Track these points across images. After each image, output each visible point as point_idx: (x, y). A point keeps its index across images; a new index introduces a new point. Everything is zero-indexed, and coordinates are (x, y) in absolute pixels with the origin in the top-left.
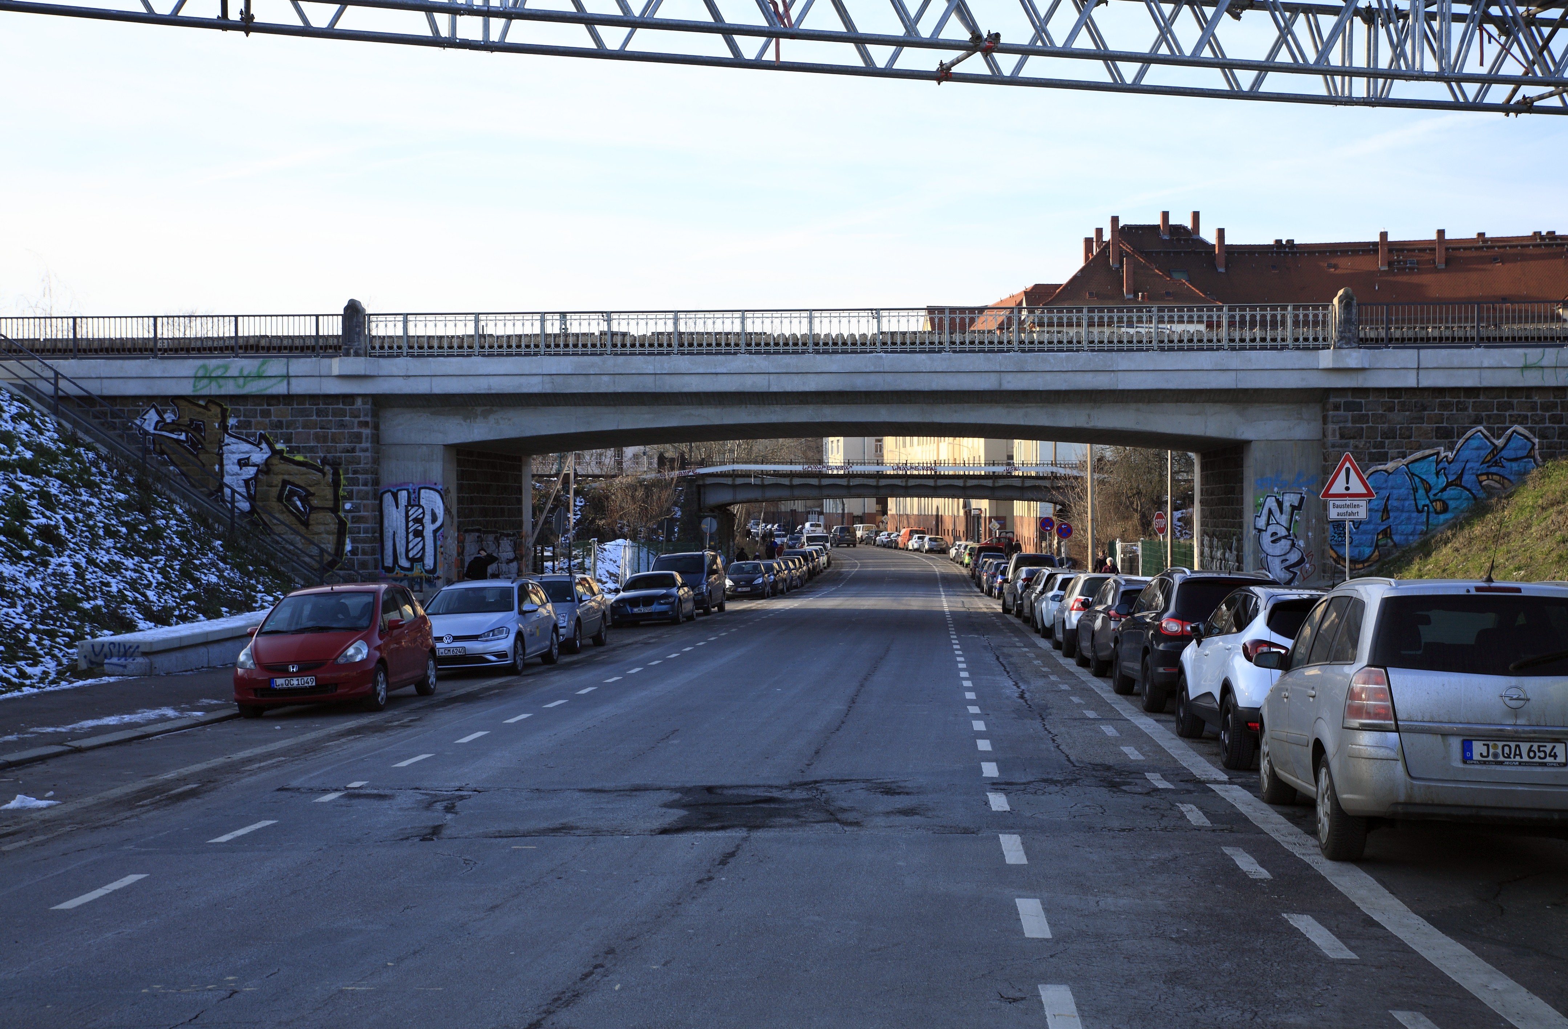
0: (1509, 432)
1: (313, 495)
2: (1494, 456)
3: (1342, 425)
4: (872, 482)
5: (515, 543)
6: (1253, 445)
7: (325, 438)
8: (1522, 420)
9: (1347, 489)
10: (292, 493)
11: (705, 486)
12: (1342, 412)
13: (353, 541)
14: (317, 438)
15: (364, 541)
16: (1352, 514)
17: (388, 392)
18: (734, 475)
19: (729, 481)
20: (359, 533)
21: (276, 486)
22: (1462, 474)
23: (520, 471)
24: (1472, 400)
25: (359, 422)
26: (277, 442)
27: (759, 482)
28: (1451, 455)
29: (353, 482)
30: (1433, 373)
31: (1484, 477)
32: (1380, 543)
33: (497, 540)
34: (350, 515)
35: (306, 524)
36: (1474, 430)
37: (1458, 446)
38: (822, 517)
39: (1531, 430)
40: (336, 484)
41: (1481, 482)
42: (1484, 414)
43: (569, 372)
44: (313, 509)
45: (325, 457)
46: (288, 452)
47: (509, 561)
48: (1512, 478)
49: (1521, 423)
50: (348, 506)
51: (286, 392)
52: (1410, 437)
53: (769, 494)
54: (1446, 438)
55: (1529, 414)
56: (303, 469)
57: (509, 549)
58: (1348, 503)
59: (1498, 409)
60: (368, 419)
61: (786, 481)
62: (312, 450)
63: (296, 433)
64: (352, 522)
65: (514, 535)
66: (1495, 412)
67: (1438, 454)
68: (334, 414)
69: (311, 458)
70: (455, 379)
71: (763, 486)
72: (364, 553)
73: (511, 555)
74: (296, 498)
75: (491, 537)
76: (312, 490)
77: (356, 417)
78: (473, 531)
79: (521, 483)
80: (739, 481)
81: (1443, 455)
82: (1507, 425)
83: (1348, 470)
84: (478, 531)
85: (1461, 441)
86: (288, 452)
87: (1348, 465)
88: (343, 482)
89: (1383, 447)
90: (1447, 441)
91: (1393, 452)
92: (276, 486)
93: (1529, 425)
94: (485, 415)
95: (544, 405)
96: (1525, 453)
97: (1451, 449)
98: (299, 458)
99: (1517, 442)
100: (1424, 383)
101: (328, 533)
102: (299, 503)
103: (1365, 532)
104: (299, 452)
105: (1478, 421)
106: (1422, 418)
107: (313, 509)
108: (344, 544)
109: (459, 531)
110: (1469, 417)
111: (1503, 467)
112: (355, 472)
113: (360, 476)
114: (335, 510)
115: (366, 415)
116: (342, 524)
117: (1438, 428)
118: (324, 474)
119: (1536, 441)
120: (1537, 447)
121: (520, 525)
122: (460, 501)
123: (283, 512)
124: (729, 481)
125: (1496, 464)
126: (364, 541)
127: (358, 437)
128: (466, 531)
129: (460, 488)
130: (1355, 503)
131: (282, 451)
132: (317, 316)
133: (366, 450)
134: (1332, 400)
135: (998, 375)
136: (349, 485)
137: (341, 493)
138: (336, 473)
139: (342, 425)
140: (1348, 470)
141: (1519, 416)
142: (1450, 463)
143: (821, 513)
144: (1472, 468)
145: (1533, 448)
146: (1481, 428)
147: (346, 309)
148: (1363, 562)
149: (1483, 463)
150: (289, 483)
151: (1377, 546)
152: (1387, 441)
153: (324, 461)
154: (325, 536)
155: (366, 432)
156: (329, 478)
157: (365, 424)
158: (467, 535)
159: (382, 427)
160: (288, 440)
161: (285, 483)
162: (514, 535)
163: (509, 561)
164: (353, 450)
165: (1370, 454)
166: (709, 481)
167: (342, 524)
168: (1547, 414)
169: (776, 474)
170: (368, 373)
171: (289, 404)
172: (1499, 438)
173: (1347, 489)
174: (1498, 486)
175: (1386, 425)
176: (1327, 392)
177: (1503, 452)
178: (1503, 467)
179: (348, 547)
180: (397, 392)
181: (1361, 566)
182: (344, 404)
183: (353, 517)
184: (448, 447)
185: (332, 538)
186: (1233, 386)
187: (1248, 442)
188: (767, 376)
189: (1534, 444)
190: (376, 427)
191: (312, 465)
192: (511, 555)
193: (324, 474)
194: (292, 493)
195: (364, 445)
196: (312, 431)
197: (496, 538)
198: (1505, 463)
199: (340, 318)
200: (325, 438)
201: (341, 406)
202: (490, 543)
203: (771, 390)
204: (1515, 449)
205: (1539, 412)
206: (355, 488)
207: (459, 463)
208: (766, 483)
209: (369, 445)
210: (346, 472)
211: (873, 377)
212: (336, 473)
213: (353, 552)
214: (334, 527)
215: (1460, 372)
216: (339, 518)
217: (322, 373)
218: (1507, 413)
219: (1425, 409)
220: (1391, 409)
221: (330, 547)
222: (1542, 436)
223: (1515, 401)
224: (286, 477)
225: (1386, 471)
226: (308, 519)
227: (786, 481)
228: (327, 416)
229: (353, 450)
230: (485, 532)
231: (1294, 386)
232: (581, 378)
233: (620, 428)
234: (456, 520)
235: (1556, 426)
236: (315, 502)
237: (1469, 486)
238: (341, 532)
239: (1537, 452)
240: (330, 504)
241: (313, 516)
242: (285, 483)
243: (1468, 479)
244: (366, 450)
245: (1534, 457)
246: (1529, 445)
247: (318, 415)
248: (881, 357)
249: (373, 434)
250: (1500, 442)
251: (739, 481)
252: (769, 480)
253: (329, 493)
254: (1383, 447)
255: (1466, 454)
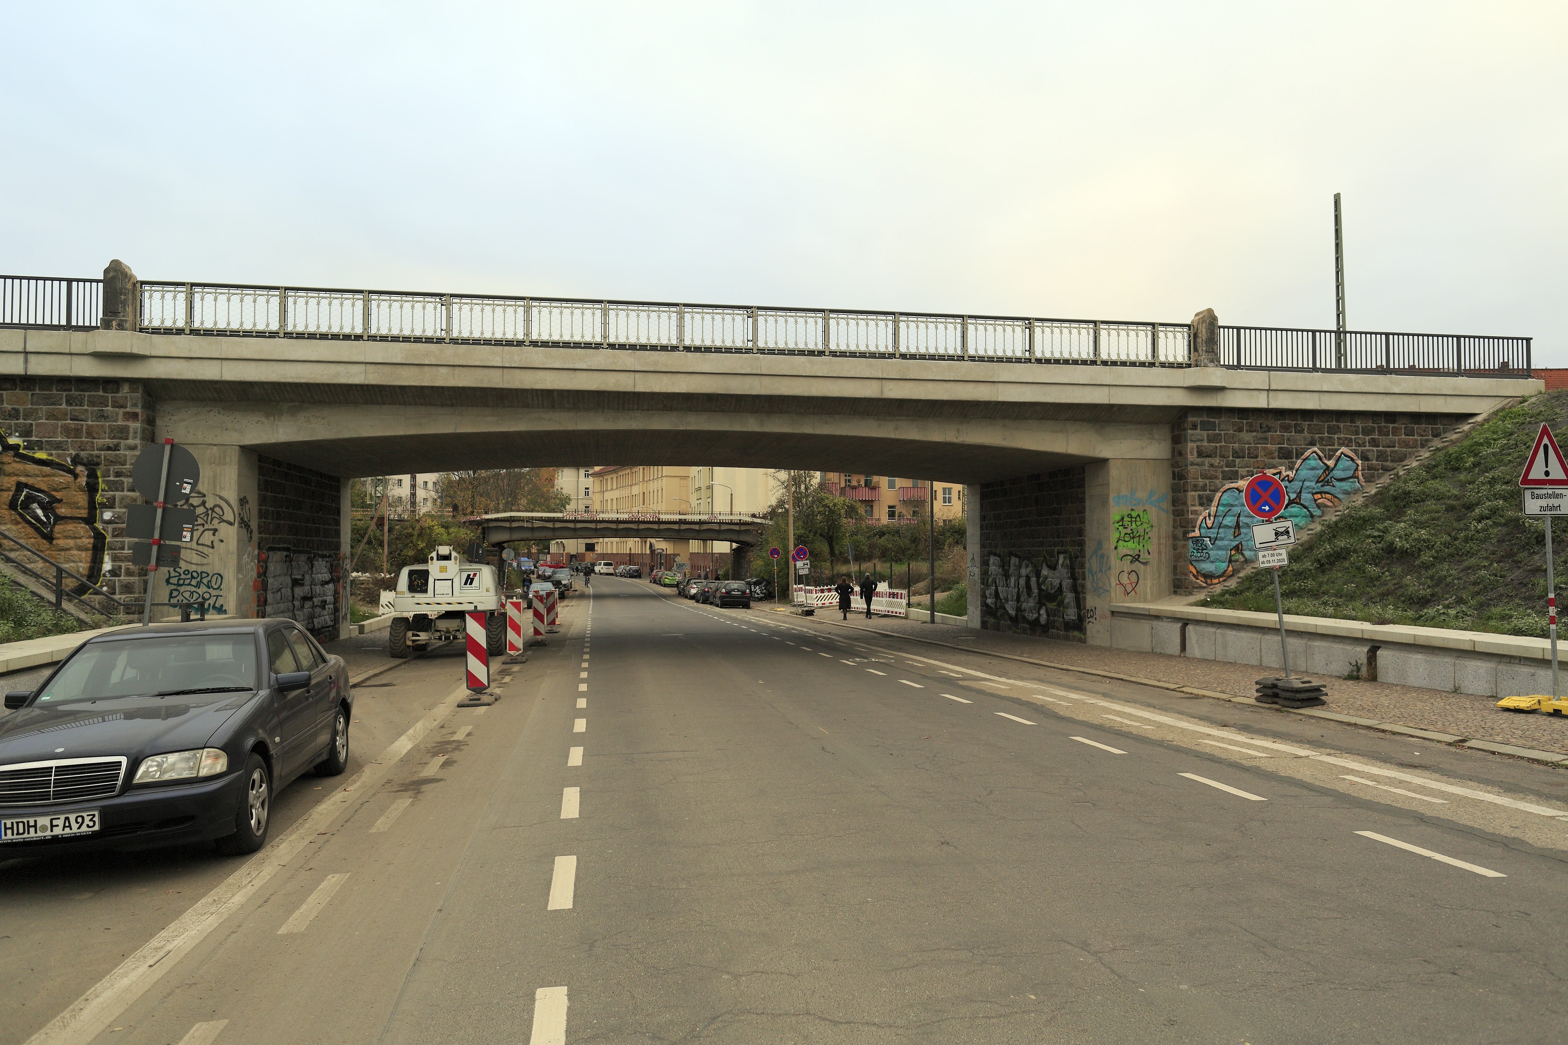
0: (1338, 453)
1: (60, 501)
2: (1327, 476)
3: (1199, 443)
4: (614, 526)
5: (332, 565)
6: (1111, 464)
7: (77, 432)
8: (1347, 443)
9: (1547, 473)
10: (30, 499)
11: (489, 528)
12: (1198, 431)
13: (114, 559)
14: (67, 431)
15: (127, 559)
16: (1553, 508)
17: (163, 376)
18: (511, 520)
19: (507, 525)
20: (123, 548)
21: (8, 490)
22: (1300, 492)
23: (339, 492)
24: (1307, 423)
25: (125, 414)
26: (10, 435)
27: (529, 525)
28: (1291, 474)
29: (115, 486)
30: (1281, 395)
31: (1319, 496)
32: (1233, 558)
33: (311, 561)
34: (110, 527)
35: (49, 538)
36: (1310, 451)
37: (1296, 466)
38: (549, 556)
39: (1355, 452)
40: (92, 489)
41: (1315, 500)
42: (1317, 436)
43: (399, 361)
44: (59, 519)
45: (77, 455)
46: (25, 448)
47: (325, 583)
48: (1341, 496)
49: (1347, 446)
50: (107, 515)
51: (22, 372)
52: (1256, 457)
53: (537, 535)
54: (1286, 458)
55: (1353, 437)
56: (47, 469)
57: (325, 570)
58: (1550, 492)
59: (1328, 433)
60: (138, 410)
61: (550, 525)
62: (58, 446)
63: (38, 425)
64: (114, 536)
65: (330, 556)
66: (1326, 434)
67: (1280, 473)
68: (92, 404)
69: (59, 456)
70: (253, 364)
71: (533, 529)
72: (129, 573)
73: (327, 576)
74: (35, 505)
75: (303, 558)
76: (58, 495)
77: (121, 407)
78: (279, 549)
79: (339, 504)
80: (515, 525)
81: (1284, 474)
82: (1336, 447)
83: (1546, 446)
84: (287, 549)
85: (1299, 461)
86: (25, 448)
87: (1546, 441)
88: (101, 486)
89: (1234, 466)
90: (1286, 461)
91: (1243, 471)
92: (8, 490)
93: (1354, 447)
94: (294, 411)
95: (366, 403)
96: (1350, 473)
97: (1291, 469)
98: (41, 455)
99: (1345, 463)
100: (1274, 405)
101: (80, 548)
102: (39, 512)
103: (1220, 548)
104: (41, 449)
105: (1313, 444)
106: (1266, 439)
107: (59, 519)
108: (101, 562)
109: (259, 548)
110: (1305, 438)
111: (1334, 486)
112: (118, 474)
113: (125, 480)
114: (90, 520)
115: (135, 405)
116: (99, 538)
117: (1280, 448)
118: (76, 476)
119: (1359, 462)
120: (1360, 468)
121: (337, 546)
122: (262, 514)
123: (18, 523)
124: (507, 525)
125: (1328, 483)
126: (127, 559)
127: (123, 433)
128: (271, 549)
129: (262, 500)
130: (1557, 491)
131: (16, 447)
132: (70, 281)
133: (133, 448)
134: (1190, 419)
135: (879, 382)
136: (110, 490)
137: (99, 498)
138: (92, 475)
139: (103, 417)
140: (1546, 446)
141: (1346, 438)
142: (1290, 482)
143: (549, 553)
144: (1308, 487)
145: (1357, 469)
146: (1315, 449)
147: (106, 271)
148: (1219, 577)
149: (1317, 482)
150: (26, 486)
151: (1230, 561)
152: (1237, 460)
153: (76, 460)
154: (75, 552)
155: (135, 426)
156: (83, 481)
157: (134, 416)
158: (271, 553)
159: (159, 422)
160: (26, 433)
161: (20, 486)
162: (330, 556)
163: (325, 583)
164: (116, 448)
165: (1223, 472)
166: (492, 525)
167: (99, 538)
168: (1367, 438)
169: (541, 519)
170: (135, 351)
171: (28, 389)
172: (1329, 459)
173: (1547, 473)
174: (1330, 504)
175: (1236, 445)
176: (1184, 411)
177: (1334, 472)
178: (1334, 486)
179: (107, 566)
180: (175, 377)
181: (1216, 581)
182: (105, 391)
183: (114, 530)
184: (244, 448)
185: (86, 556)
186: (1106, 402)
187: (1105, 461)
188: (632, 375)
189: (1358, 465)
190: (151, 422)
191: (58, 464)
192: (327, 576)
193: (76, 476)
194: (30, 499)
195: (130, 442)
196: (60, 423)
197: (309, 558)
198: (1337, 484)
199: (101, 285)
200: (77, 432)
201: (101, 393)
202: (302, 564)
203: (637, 390)
204: (1344, 470)
205: (1361, 436)
206: (118, 494)
207: (262, 471)
208: (535, 526)
209: (138, 442)
210: (106, 474)
211: (748, 379)
212: (92, 475)
213: (114, 572)
214: (88, 542)
215: (1303, 394)
216: (95, 530)
217: (73, 351)
218: (1336, 436)
219: (1269, 430)
220: (1240, 430)
221: (83, 567)
222: (1365, 458)
223: (1342, 425)
224: (23, 479)
225: (1237, 489)
226: (52, 531)
227: (550, 525)
228: (81, 405)
229: (116, 448)
230: (295, 552)
231: (1161, 404)
232: (414, 369)
233: (458, 431)
234: (256, 535)
235: (1375, 449)
236: (62, 511)
237: (1306, 504)
238: (98, 547)
239: (1360, 473)
240: (84, 513)
241: (57, 528)
242: (20, 486)
243: (1306, 497)
244: (133, 448)
245: (1357, 478)
246: (1354, 466)
247: (68, 403)
248: (758, 358)
249: (144, 430)
250: (1331, 463)
251: (515, 525)
252: (537, 524)
253: (82, 499)
254: (1234, 466)
255: (1304, 473)
